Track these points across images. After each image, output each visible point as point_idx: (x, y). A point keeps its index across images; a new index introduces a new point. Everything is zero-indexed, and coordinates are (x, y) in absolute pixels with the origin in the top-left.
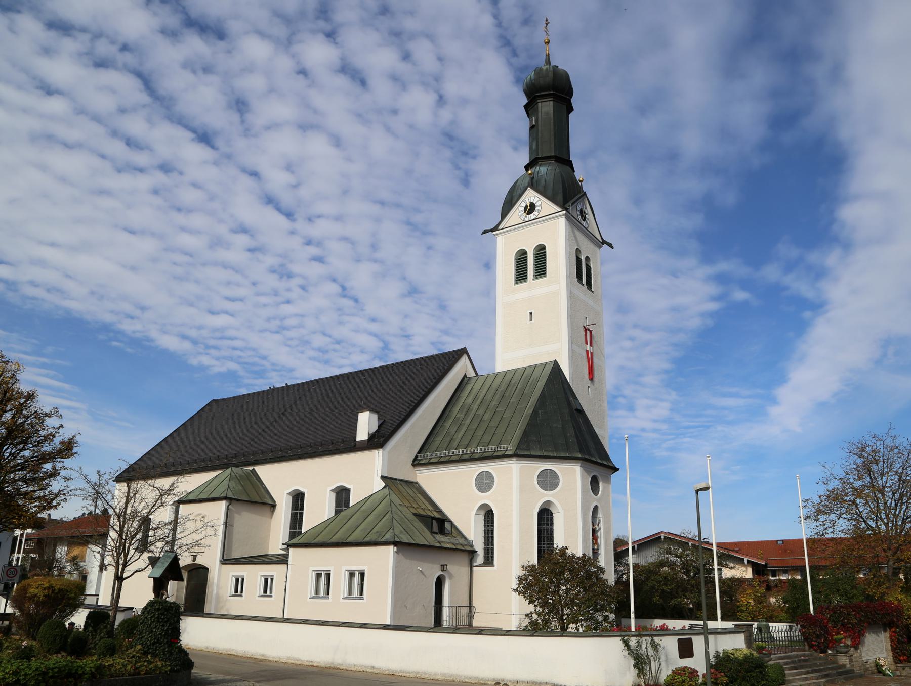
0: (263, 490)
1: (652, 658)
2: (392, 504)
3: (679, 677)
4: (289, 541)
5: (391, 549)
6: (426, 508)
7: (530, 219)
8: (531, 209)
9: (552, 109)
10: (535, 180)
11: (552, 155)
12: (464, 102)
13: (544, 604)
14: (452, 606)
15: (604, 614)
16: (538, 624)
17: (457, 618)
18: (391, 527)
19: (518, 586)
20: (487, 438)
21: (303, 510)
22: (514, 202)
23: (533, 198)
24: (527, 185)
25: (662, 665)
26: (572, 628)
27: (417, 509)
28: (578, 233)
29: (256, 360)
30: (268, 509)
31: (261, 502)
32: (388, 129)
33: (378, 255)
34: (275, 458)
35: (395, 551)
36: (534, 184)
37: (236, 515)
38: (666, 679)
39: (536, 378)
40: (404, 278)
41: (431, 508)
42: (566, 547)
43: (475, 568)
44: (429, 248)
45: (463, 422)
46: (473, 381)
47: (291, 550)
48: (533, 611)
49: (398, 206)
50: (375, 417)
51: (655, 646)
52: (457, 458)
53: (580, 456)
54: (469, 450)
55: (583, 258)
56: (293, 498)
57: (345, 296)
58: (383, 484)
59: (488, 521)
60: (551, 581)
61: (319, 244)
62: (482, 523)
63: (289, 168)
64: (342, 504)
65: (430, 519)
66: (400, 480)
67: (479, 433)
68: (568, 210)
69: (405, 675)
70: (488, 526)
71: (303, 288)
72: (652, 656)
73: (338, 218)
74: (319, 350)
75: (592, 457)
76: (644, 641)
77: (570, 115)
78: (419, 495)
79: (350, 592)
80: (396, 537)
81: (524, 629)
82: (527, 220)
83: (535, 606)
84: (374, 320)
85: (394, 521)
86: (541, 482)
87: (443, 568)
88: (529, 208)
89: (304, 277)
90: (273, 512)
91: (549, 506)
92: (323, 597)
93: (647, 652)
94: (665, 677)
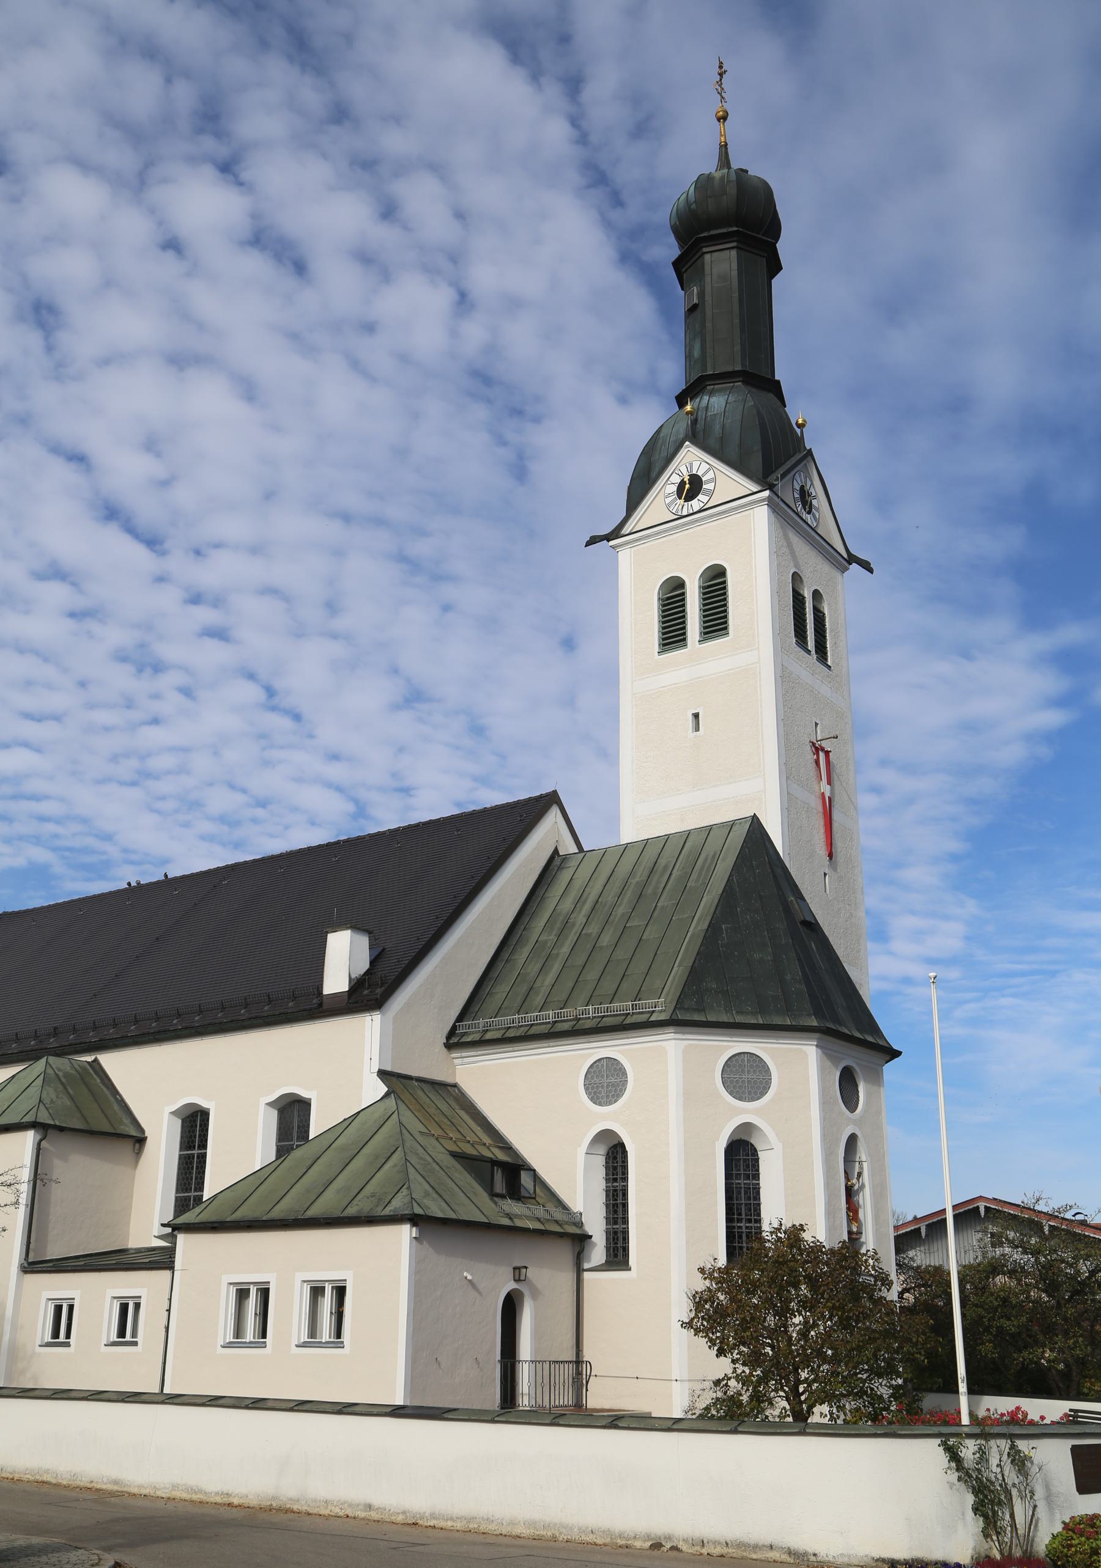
0: (116, 1107)
1: (1014, 1492)
2: (404, 1131)
3: (1083, 1539)
4: (175, 1218)
5: (405, 1232)
6: (478, 1140)
7: (691, 512)
8: (692, 488)
9: (735, 266)
10: (700, 426)
11: (736, 369)
12: (513, 304)
13: (754, 1359)
14: (539, 1362)
15: (894, 1382)
16: (740, 1404)
17: (552, 1388)
18: (404, 1183)
19: (693, 1315)
20: (608, 986)
21: (206, 1149)
22: (653, 475)
23: (696, 465)
24: (681, 436)
25: (1038, 1510)
26: (821, 1414)
27: (459, 1144)
28: (795, 540)
29: (91, 842)
30: (128, 1147)
31: (114, 1132)
32: (355, 365)
33: (340, 624)
34: (143, 1034)
35: (414, 1235)
36: (699, 434)
37: (57, 1162)
38: (1051, 1543)
39: (712, 853)
40: (395, 671)
41: (487, 1140)
42: (801, 1225)
43: (587, 1276)
44: (447, 608)
45: (554, 952)
46: (573, 863)
47: (182, 1238)
48: (729, 1372)
49: (378, 522)
50: (364, 941)
51: (1020, 1462)
52: (544, 1029)
53: (815, 1023)
54: (569, 1012)
55: (807, 594)
56: (183, 1121)
57: (274, 709)
58: (383, 1089)
59: (615, 1168)
60: (768, 1302)
61: (217, 602)
62: (602, 1172)
63: (151, 445)
64: (291, 1134)
65: (490, 1164)
66: (420, 1080)
67: (592, 975)
68: (774, 489)
69: (442, 1524)
70: (615, 1180)
71: (187, 692)
72: (1014, 1485)
73: (256, 550)
74: (222, 819)
75: (840, 1024)
76: (994, 1450)
77: (773, 281)
78: (462, 1113)
79: (313, 1331)
80: (415, 1204)
81: (700, 1415)
82: (685, 513)
83: (734, 1361)
84: (334, 757)
85: (411, 1170)
86: (732, 1082)
87: (518, 1273)
88: (687, 486)
89: (185, 669)
90: (139, 1153)
91: (750, 1135)
92: (251, 1342)
93: (1003, 1475)
94: (1047, 1540)
